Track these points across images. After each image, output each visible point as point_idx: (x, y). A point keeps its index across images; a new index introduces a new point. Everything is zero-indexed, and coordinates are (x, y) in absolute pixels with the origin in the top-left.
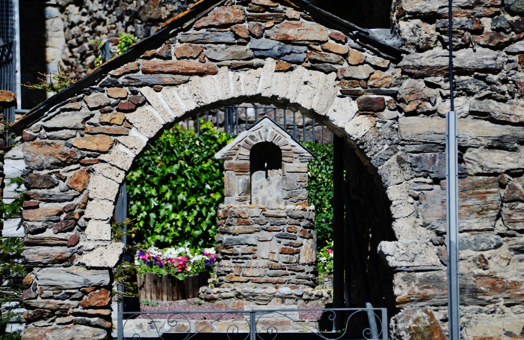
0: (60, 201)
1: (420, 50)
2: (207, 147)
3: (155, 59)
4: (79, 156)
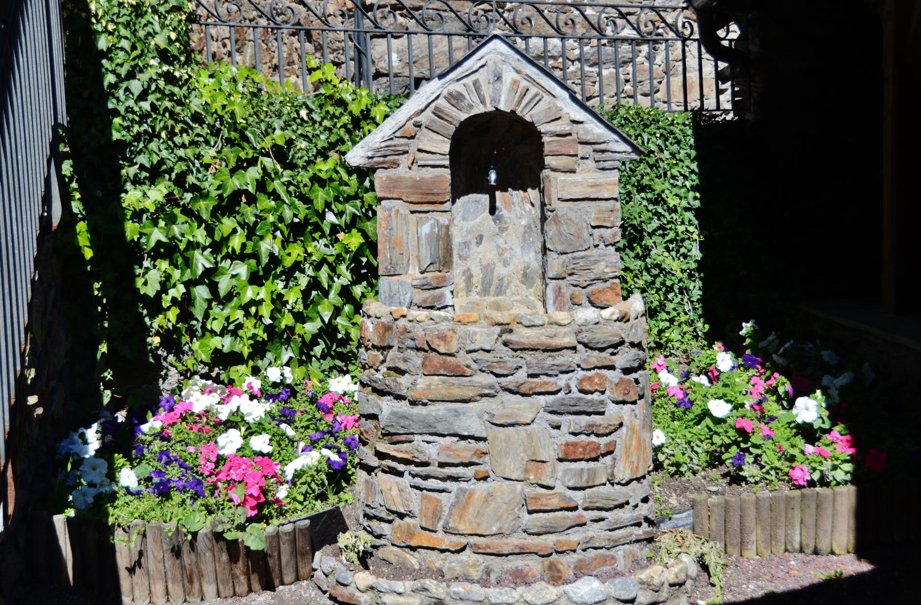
2: (326, 123)
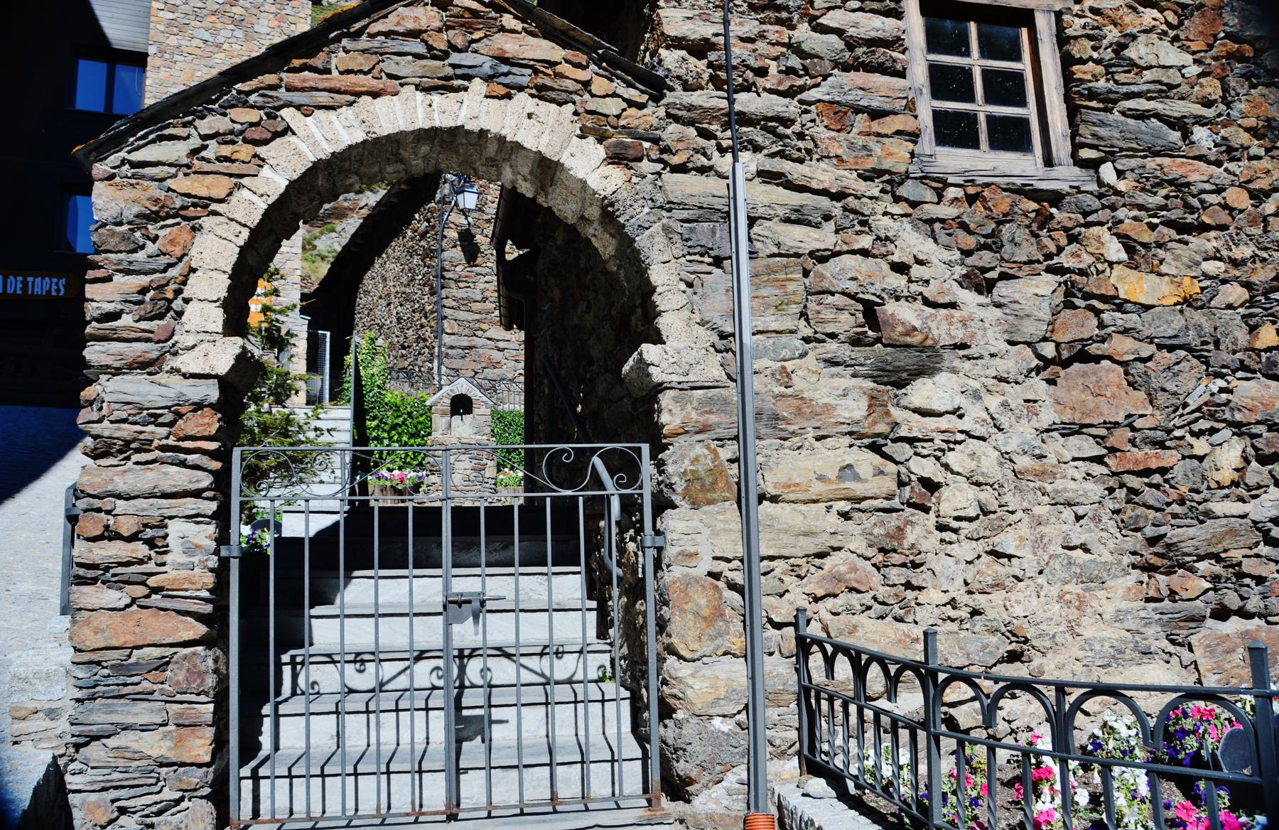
0: (146, 273)
1: (687, 87)
3: (306, 73)
4: (178, 205)
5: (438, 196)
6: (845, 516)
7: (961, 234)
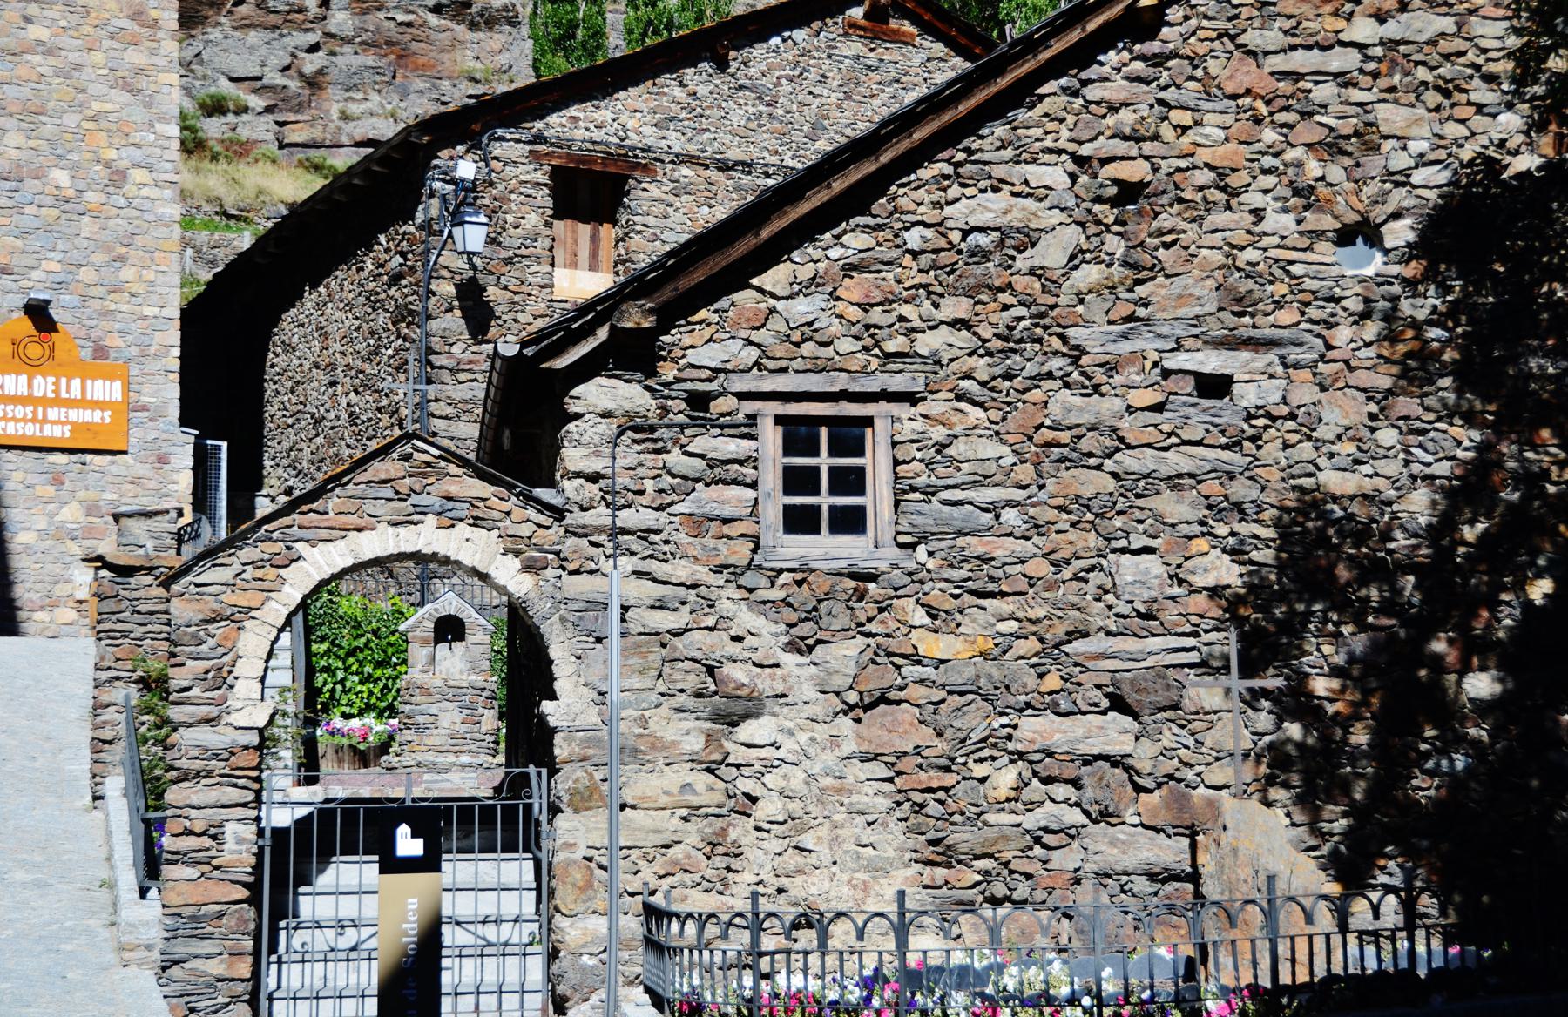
1: (583, 509)
5: (420, 217)
6: (685, 819)
7: (786, 611)
